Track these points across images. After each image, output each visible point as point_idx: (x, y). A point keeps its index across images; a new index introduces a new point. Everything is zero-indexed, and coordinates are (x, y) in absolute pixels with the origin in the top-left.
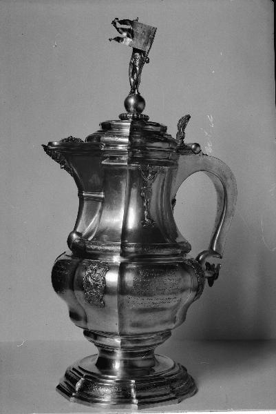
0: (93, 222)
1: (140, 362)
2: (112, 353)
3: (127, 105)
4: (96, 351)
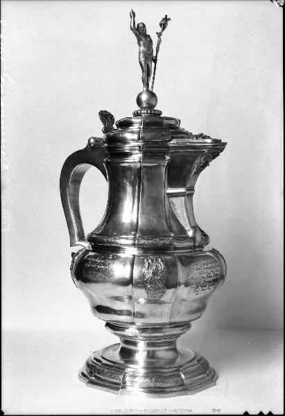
0: (141, 338)
1: (163, 353)
2: (135, 344)
3: (139, 102)
4: (117, 340)
